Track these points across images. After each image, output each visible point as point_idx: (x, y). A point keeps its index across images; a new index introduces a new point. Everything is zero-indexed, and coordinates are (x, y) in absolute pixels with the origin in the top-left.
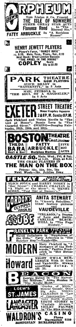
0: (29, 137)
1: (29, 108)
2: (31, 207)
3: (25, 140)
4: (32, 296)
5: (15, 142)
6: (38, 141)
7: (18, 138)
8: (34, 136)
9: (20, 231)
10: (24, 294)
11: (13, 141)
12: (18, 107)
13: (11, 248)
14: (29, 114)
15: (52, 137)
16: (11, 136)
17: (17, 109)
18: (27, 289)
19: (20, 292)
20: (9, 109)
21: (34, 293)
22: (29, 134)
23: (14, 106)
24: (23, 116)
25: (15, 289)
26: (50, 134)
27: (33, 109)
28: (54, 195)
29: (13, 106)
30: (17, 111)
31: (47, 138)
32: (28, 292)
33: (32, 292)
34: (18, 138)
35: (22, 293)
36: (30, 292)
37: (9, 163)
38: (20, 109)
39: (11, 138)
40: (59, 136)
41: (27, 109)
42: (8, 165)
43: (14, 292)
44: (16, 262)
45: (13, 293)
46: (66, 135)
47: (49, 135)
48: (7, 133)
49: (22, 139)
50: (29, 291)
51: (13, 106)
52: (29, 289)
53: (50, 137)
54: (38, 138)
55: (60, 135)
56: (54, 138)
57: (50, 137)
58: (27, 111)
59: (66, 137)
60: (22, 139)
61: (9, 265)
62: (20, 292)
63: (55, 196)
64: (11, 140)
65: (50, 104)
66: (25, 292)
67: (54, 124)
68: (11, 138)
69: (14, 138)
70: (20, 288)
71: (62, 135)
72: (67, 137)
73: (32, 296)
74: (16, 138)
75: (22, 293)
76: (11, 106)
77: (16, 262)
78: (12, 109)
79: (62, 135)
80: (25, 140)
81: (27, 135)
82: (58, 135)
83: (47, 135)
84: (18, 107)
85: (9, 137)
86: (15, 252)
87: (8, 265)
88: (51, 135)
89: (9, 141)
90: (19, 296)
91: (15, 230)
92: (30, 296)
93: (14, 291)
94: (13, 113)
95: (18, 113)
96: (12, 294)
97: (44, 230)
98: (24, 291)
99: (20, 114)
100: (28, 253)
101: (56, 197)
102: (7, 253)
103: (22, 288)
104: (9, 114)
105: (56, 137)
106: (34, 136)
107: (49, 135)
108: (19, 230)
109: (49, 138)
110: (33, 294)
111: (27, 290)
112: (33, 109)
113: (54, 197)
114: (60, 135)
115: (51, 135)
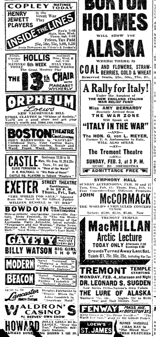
0: (31, 132)
1: (31, 184)
2: (77, 179)
3: (26, 135)
4: (107, 332)
5: (16, 138)
6: (41, 137)
7: (19, 134)
8: (36, 132)
10: (99, 331)
12: (19, 183)
13: (106, 199)
14: (31, 189)
15: (56, 133)
17: (18, 184)
18: (102, 325)
19: (94, 328)
20: (9, 184)
21: (109, 330)
22: (31, 129)
23: (15, 181)
24: (24, 192)
25: (88, 325)
26: (53, 130)
28: (97, 178)
29: (13, 182)
30: (18, 187)
31: (51, 134)
32: (103, 329)
33: (107, 328)
34: (19, 134)
35: (97, 329)
36: (105, 329)
37: (12, 76)
38: (21, 184)
39: (12, 134)
40: (63, 132)
42: (12, 79)
43: (88, 328)
44: (17, 321)
45: (87, 329)
46: (70, 131)
47: (52, 131)
49: (24, 134)
50: (104, 327)
51: (13, 182)
52: (105, 325)
53: (53, 132)
54: (40, 133)
55: (64, 131)
56: (57, 134)
57: (53, 132)
58: (29, 187)
59: (70, 133)
60: (24, 134)
61: (9, 327)
62: (94, 328)
64: (12, 135)
65: (20, 182)
66: (100, 328)
69: (15, 133)
70: (94, 323)
71: (66, 131)
72: (72, 133)
73: (107, 332)
74: (17, 133)
75: (97, 329)
76: (12, 182)
77: (17, 321)
78: (13, 185)
79: (66, 131)
80: (26, 135)
81: (28, 130)
82: (61, 131)
83: (50, 130)
84: (19, 183)
85: (9, 133)
87: (8, 327)
88: (55, 131)
89: (10, 137)
90: (94, 332)
92: (106, 332)
93: (87, 327)
94: (13, 188)
95: (19, 188)
96: (85, 330)
98: (98, 327)
99: (21, 190)
102: (101, 203)
103: (96, 324)
104: (9, 190)
105: (60, 133)
106: (36, 132)
107: (52, 131)
109: (52, 134)
110: (108, 331)
111: (102, 327)
112: (35, 185)
114: (64, 131)
115: (55, 131)
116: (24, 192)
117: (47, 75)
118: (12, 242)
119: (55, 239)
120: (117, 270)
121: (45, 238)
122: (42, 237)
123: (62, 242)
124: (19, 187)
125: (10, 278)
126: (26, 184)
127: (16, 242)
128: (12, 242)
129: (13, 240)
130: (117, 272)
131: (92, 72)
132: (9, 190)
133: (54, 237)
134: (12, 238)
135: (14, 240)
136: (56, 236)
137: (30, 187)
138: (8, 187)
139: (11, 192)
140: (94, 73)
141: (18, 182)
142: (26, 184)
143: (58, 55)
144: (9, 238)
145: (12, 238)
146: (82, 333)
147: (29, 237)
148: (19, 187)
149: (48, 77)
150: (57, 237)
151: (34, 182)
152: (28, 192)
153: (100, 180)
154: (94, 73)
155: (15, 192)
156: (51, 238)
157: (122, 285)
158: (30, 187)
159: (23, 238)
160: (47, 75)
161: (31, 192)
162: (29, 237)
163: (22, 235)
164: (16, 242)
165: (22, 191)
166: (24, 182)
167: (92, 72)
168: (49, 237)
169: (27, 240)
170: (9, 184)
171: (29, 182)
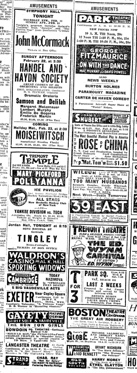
0: (88, 312)
1: (28, 295)
3: (84, 314)
7: (78, 312)
9: (22, 359)
11: (73, 315)
12: (18, 294)
14: (28, 299)
16: (71, 311)
20: (10, 295)
27: (32, 296)
34: (78, 312)
41: (26, 295)
48: (69, 308)
54: (96, 313)
58: (27, 297)
63: (23, 344)
65: (19, 292)
67: (52, 306)
68: (72, 312)
76: (12, 292)
78: (13, 295)
80: (84, 314)
84: (18, 294)
85: (70, 312)
86: (134, 364)
91: (17, 358)
94: (13, 298)
97: (24, 359)
99: (20, 299)
100: (30, 301)
101: (24, 345)
104: (10, 299)
105: (113, 313)
107: (106, 311)
108: (20, 358)
112: (32, 296)
113: (22, 345)
116: (23, 301)
117: (64, 100)
118: (11, 317)
119: (48, 314)
120: (103, 314)
121: (40, 314)
122: (37, 313)
123: (53, 315)
124: (19, 297)
125: (22, 280)
126: (24, 294)
127: (14, 317)
128: (11, 317)
129: (11, 316)
130: (102, 315)
131: (21, 80)
132: (10, 299)
133: (46, 313)
134: (11, 314)
135: (12, 316)
136: (48, 311)
137: (28, 297)
138: (9, 297)
139: (12, 301)
140: (23, 81)
141: (18, 293)
142: (24, 294)
143: (103, 304)
144: (9, 314)
145: (11, 314)
146: (63, 253)
147: (25, 313)
148: (19, 297)
149: (65, 101)
150: (49, 312)
151: (31, 293)
152: (26, 301)
153: (31, 11)
154: (23, 81)
155: (15, 301)
156: (45, 314)
157: (94, 263)
158: (28, 297)
159: (20, 314)
160: (64, 100)
161: (28, 301)
162: (25, 313)
163: (19, 311)
164: (14, 317)
165: (21, 301)
166: (23, 293)
167: (21, 80)
168: (43, 313)
169: (23, 315)
170: (10, 295)
171: (27, 293)
